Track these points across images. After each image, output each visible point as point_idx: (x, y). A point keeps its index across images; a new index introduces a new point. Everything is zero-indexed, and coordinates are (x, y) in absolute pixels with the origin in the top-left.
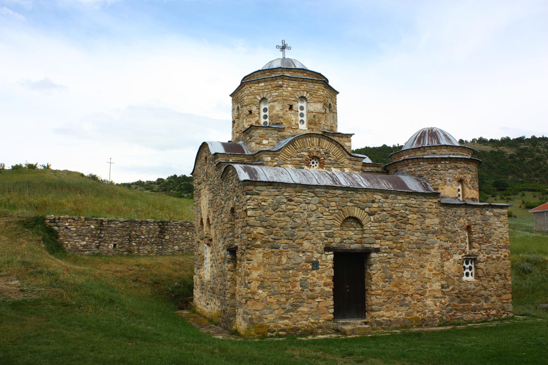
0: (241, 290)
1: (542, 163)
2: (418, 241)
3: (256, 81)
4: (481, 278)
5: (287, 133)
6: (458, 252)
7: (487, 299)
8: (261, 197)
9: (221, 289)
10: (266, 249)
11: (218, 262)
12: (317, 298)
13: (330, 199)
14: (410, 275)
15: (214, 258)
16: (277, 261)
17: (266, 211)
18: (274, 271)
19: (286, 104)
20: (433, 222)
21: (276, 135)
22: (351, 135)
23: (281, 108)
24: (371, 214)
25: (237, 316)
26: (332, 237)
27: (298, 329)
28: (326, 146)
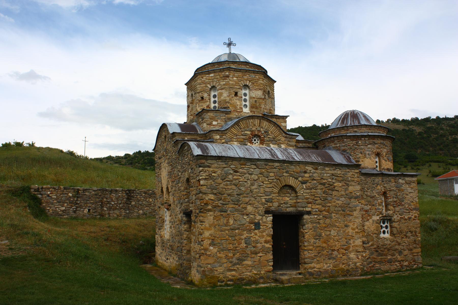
0: (195, 247)
1: (445, 139)
2: (343, 205)
3: (207, 73)
4: (396, 236)
5: (233, 115)
6: (376, 214)
7: (400, 253)
8: (211, 169)
9: (178, 247)
10: (216, 212)
11: (176, 224)
12: (259, 253)
13: (269, 170)
14: (336, 234)
15: (172, 220)
16: (225, 222)
17: (216, 181)
18: (223, 231)
19: (232, 91)
20: (355, 188)
21: (224, 118)
22: (287, 117)
23: (228, 95)
24: (303, 183)
25: (192, 269)
26: (271, 202)
27: (243, 279)
28: (266, 126)
